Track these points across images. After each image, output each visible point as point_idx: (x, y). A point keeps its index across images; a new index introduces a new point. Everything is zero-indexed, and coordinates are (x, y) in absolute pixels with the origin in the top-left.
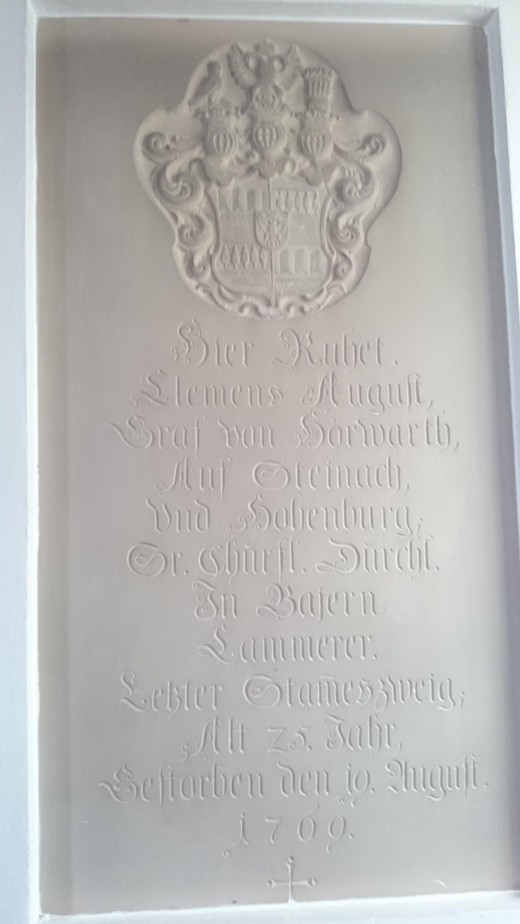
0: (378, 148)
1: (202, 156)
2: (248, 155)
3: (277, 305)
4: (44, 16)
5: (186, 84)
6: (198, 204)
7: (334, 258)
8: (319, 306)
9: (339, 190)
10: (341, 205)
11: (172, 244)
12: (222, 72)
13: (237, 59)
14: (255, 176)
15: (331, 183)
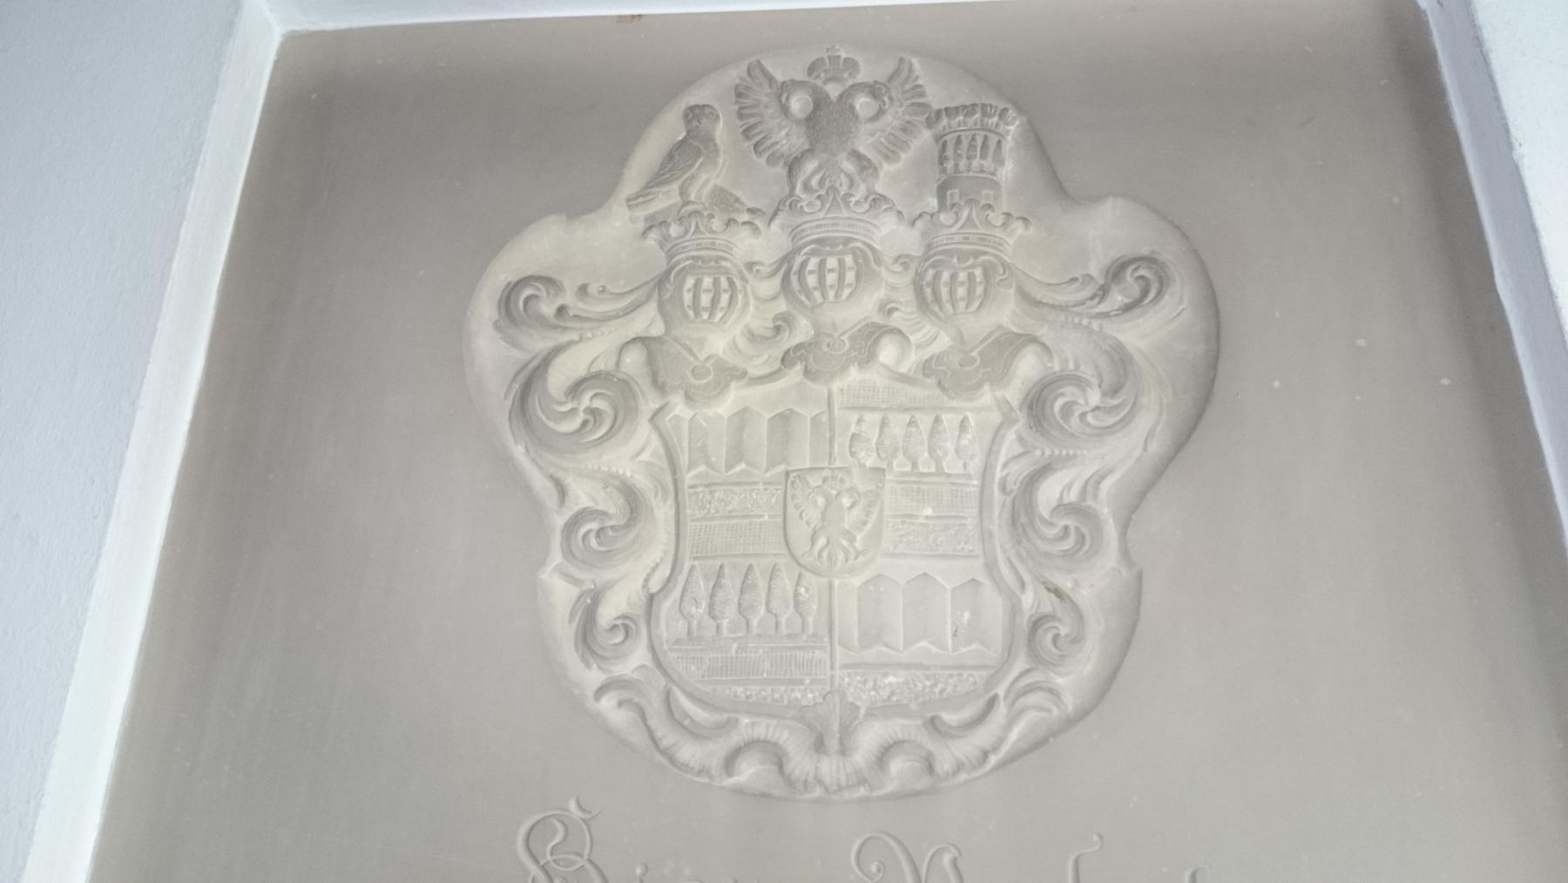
0: (1145, 293)
1: (658, 329)
2: (782, 324)
3: (844, 751)
4: (297, 28)
5: (623, 161)
6: (632, 455)
7: (1027, 600)
8: (985, 754)
9: (1037, 404)
10: (1044, 450)
11: (542, 562)
12: (721, 131)
13: (763, 94)
14: (795, 375)
15: (1014, 393)
